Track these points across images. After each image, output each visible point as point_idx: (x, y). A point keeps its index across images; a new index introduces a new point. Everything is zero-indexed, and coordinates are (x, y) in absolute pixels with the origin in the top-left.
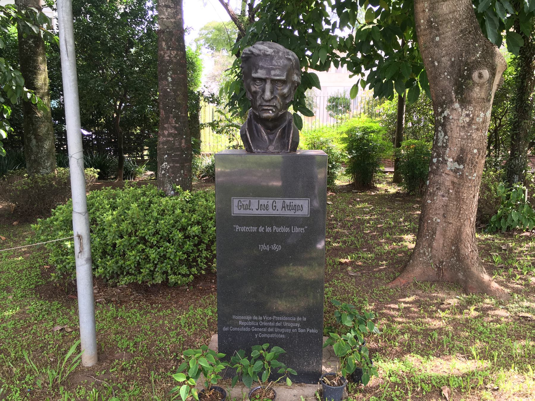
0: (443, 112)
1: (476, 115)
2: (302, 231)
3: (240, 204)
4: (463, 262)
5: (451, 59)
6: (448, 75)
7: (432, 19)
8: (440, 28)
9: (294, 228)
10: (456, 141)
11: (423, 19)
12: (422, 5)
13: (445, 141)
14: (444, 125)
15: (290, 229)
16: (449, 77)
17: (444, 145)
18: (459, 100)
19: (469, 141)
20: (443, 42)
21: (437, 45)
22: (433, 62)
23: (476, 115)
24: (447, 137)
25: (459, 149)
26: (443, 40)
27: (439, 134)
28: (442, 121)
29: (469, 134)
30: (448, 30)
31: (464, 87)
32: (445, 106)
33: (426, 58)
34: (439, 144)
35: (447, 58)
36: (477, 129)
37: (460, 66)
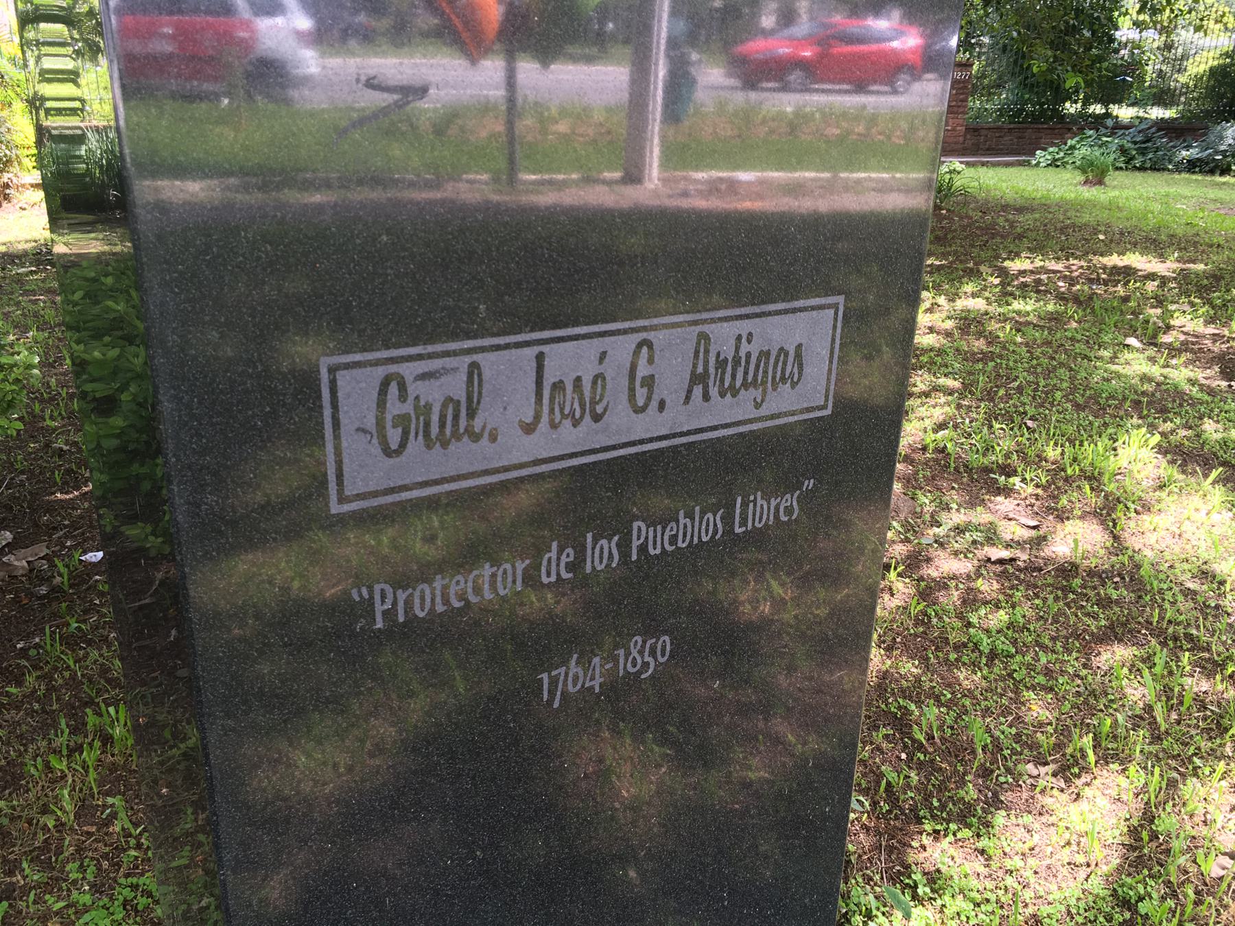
2: (789, 510)
9: (745, 505)
15: (728, 519)
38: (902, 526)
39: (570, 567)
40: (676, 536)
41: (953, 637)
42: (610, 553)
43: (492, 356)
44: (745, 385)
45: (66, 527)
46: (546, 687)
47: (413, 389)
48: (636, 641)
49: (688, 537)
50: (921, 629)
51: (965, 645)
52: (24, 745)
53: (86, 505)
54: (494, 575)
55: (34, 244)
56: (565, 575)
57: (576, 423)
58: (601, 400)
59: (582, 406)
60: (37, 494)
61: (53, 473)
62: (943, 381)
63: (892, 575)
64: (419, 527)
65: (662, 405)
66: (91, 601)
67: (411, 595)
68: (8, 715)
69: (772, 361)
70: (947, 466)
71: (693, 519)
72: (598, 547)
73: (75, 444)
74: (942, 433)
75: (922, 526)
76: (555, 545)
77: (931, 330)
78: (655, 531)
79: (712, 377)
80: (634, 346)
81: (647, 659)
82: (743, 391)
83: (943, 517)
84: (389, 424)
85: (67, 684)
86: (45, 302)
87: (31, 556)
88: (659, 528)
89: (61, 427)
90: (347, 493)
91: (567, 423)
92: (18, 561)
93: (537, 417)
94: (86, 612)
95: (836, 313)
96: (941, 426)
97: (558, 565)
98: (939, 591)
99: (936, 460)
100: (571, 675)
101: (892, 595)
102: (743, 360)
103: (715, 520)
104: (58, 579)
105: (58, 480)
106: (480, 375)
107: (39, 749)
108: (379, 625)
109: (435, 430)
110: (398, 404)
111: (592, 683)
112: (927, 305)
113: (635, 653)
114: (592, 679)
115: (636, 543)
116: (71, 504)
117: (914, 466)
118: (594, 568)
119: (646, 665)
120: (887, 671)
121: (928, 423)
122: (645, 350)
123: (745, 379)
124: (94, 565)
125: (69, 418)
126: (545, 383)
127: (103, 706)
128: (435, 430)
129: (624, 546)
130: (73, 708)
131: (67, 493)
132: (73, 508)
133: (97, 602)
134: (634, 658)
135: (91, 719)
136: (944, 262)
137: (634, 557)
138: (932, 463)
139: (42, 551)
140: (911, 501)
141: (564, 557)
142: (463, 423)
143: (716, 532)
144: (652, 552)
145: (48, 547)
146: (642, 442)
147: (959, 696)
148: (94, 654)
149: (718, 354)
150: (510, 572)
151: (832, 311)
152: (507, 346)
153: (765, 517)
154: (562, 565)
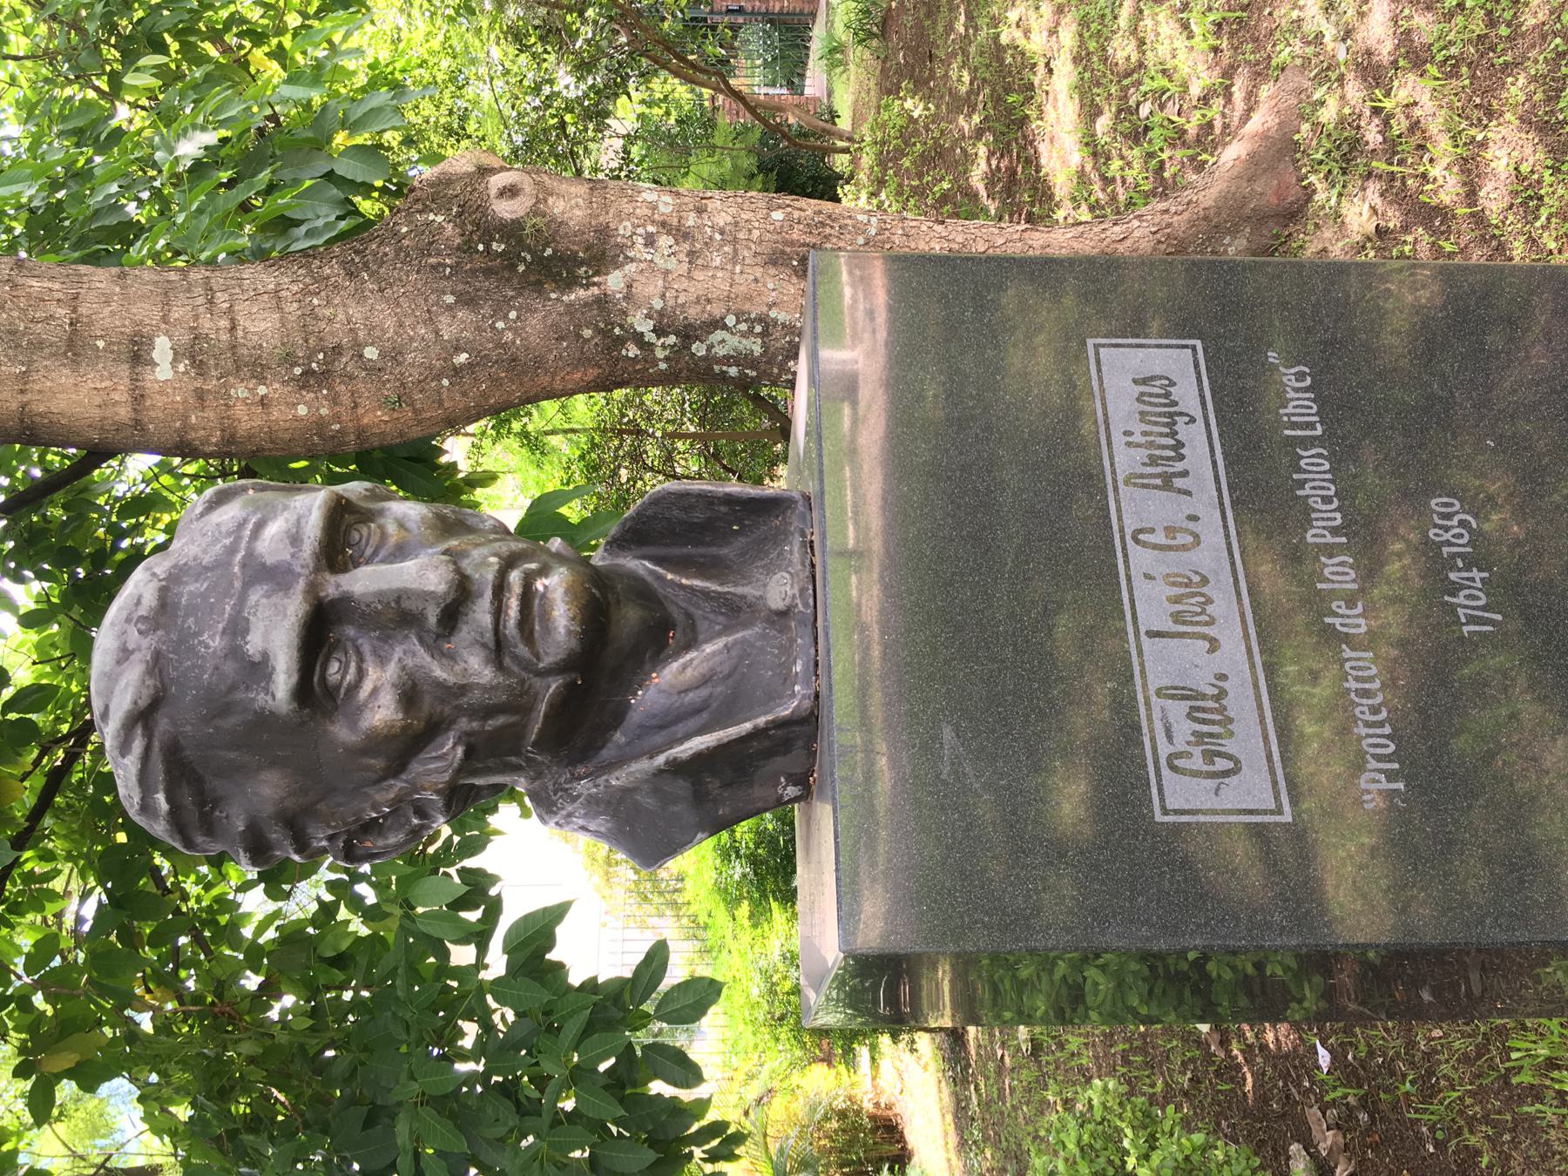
0: (638, 338)
1: (649, 213)
2: (1300, 376)
3: (1197, 762)
4: (1182, 241)
5: (449, 308)
6: (505, 317)
7: (298, 371)
8: (330, 342)
9: (1294, 426)
10: (743, 285)
11: (295, 405)
12: (239, 411)
13: (743, 327)
14: (688, 334)
15: (1306, 443)
16: (513, 315)
17: (758, 329)
18: (597, 273)
19: (741, 235)
20: (384, 332)
21: (394, 354)
22: (457, 371)
23: (649, 213)
24: (730, 320)
25: (772, 271)
26: (378, 333)
27: (720, 351)
28: (672, 339)
29: (718, 237)
30: (341, 317)
31: (549, 251)
32: (617, 331)
33: (441, 403)
34: (757, 350)
35: (444, 320)
36: (700, 211)
37: (473, 272)
38: (1320, 85)
39: (1351, 604)
40: (1323, 497)
41: (1478, 27)
42: (1339, 564)
43: (1150, 677)
44: (1173, 434)
45: (1286, 1085)
46: (1477, 628)
47: (1180, 745)
48: (1435, 535)
49: (1325, 484)
50: (1464, 70)
51: (1489, 13)
52: (1554, 1155)
53: (1259, 1060)
54: (1357, 679)
55: (943, 1084)
56: (1360, 609)
57: (1209, 601)
58: (1188, 578)
59: (1193, 595)
60: (1245, 1111)
61: (1220, 1091)
62: (1123, 22)
63: (1388, 104)
64: (1297, 688)
65: (1193, 518)
66: (1379, 1067)
67: (1373, 756)
68: (1516, 1165)
69: (1149, 409)
70: (1240, 20)
71: (1306, 481)
72: (1331, 577)
73: (1183, 1063)
74: (1193, 27)
75: (1322, 58)
76: (1327, 620)
77: (1053, 32)
78: (1317, 519)
79: (1166, 469)
80: (1138, 547)
81: (1455, 522)
82: (1178, 437)
83: (1309, 28)
84: (1211, 768)
85: (1481, 1102)
86: (1013, 1079)
87: (1321, 1125)
88: (1314, 515)
89: (1164, 1078)
90: (1273, 807)
91: (1209, 609)
92: (1327, 1140)
93: (1204, 637)
94: (1392, 1074)
95: (1104, 346)
96: (1185, 26)
97: (1348, 617)
98: (1412, 41)
99: (1232, 35)
100: (1467, 603)
101: (1415, 103)
102: (1148, 438)
103: (1307, 457)
104: (1350, 1099)
105: (1227, 1087)
106: (1167, 688)
107: (1559, 1139)
108: (1401, 786)
109: (1216, 729)
110: (1194, 758)
111: (1478, 580)
112: (1018, 34)
113: (1448, 536)
114: (1473, 580)
115: (1330, 539)
116: (1259, 1077)
117: (1239, 66)
118: (1354, 581)
119: (1462, 524)
120: (1520, 118)
121: (1181, 43)
122: (1141, 537)
123: (1167, 435)
124: (1334, 1059)
125: (1152, 1067)
126: (1174, 630)
127: (1508, 1064)
128: (1216, 729)
129: (1330, 550)
130: (1511, 1098)
131: (1245, 1079)
132: (1264, 1074)
133: (1381, 1060)
134: (1453, 536)
135: (1526, 1078)
136: (962, 10)
137: (1344, 540)
138: (1235, 41)
139: (1315, 1114)
140: (1287, 72)
141: (1340, 611)
142: (1211, 704)
143: (1319, 455)
144: (1339, 522)
145: (1311, 1107)
146: (1227, 536)
147: (1558, 25)
148: (1445, 1068)
149: (1144, 464)
150: (1353, 663)
151: (1101, 350)
152: (1142, 665)
153: (1306, 403)
154: (1349, 612)
